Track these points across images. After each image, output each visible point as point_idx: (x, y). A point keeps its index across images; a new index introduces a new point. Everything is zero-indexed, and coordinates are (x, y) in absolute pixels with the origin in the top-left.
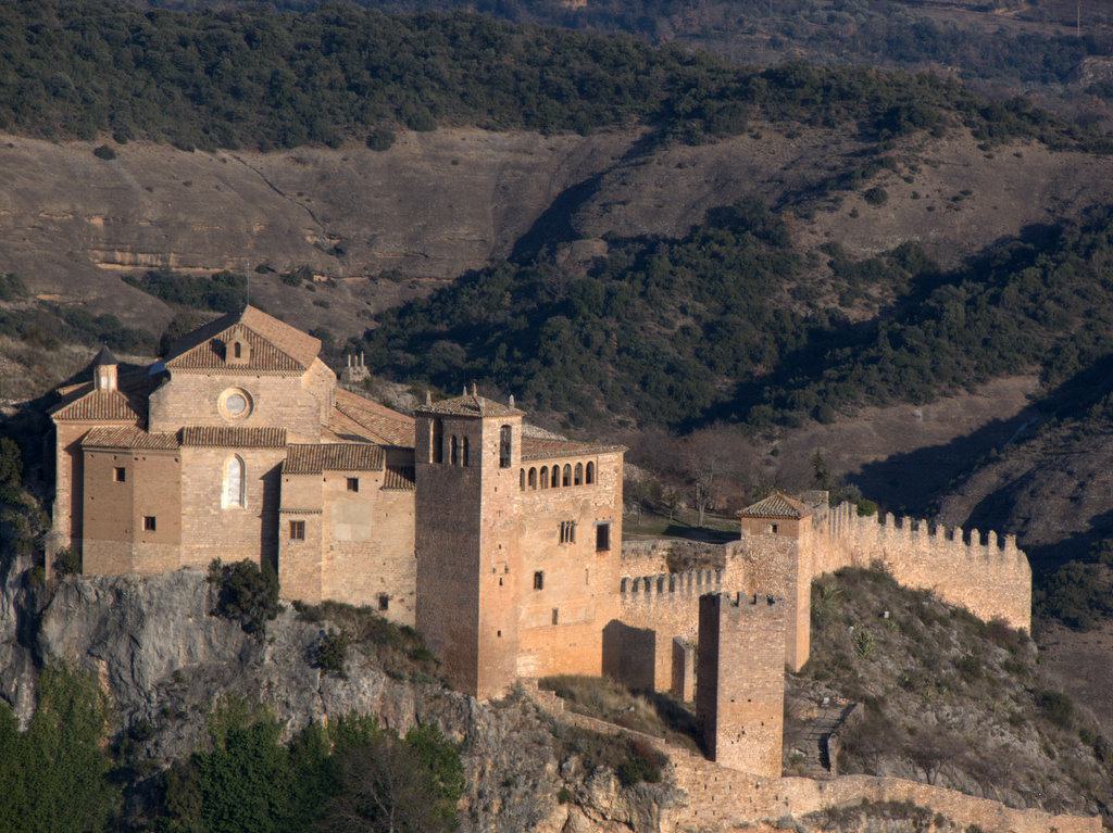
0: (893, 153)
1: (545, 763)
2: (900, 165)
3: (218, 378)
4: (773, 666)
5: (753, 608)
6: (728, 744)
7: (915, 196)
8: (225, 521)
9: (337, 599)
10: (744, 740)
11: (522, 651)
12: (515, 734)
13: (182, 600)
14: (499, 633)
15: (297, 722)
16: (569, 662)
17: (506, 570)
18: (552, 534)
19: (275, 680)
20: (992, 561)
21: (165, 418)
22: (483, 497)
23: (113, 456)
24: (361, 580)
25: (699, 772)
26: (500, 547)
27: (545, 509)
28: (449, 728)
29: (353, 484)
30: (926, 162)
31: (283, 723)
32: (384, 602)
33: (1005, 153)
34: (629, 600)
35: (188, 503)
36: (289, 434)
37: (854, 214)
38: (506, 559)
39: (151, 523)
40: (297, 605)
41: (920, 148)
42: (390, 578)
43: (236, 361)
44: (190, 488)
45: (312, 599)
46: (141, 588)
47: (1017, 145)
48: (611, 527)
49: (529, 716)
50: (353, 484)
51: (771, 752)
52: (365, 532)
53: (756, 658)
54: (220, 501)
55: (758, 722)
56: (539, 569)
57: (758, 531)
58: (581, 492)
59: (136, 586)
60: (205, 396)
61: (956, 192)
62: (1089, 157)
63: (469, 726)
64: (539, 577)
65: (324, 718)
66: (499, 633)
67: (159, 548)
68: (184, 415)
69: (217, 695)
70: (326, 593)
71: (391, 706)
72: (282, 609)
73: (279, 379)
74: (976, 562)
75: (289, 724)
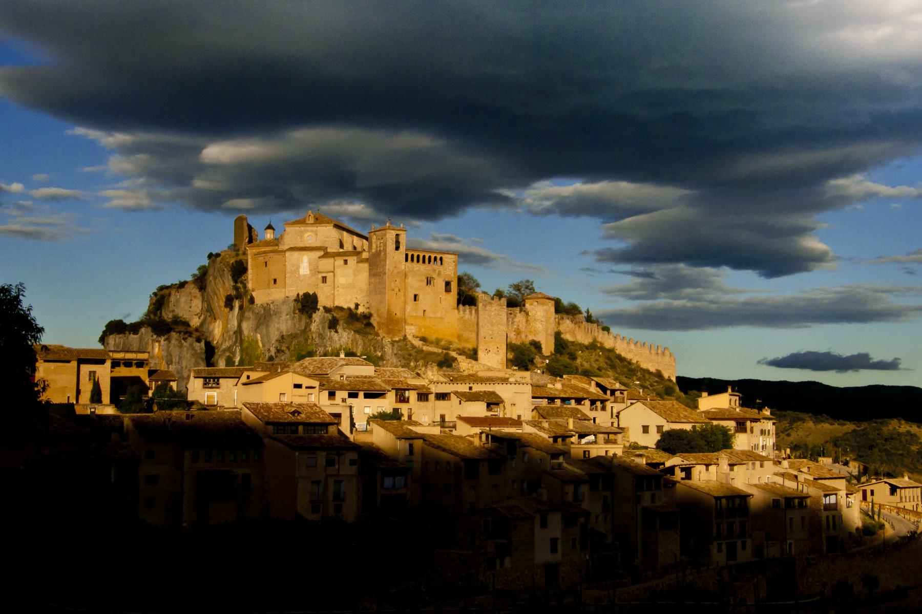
0: (793, 426)
1: (410, 362)
2: (794, 429)
3: (303, 228)
4: (501, 325)
5: (493, 302)
6: (483, 355)
7: (798, 435)
8: (301, 279)
9: (340, 305)
10: (490, 354)
11: (408, 324)
12: (400, 352)
13: (285, 309)
14: (396, 314)
15: (322, 351)
16: (432, 332)
17: (399, 290)
18: (423, 281)
19: (314, 336)
20: (660, 355)
21: (284, 244)
22: (387, 260)
23: (263, 258)
24: (349, 298)
25: (470, 365)
26: (396, 281)
27: (418, 270)
28: (375, 351)
29: (346, 262)
30: (801, 428)
31: (316, 351)
32: (357, 305)
33: (820, 426)
34: (461, 312)
35: (288, 273)
36: (328, 248)
37: (783, 438)
38: (399, 286)
39: (275, 281)
40: (325, 308)
41: (800, 425)
42: (359, 297)
43: (309, 222)
44: (289, 267)
45: (329, 304)
46: (271, 306)
47: (823, 424)
48: (452, 283)
49: (407, 347)
50: (346, 262)
51: (502, 359)
52: (350, 280)
53: (494, 321)
54: (299, 272)
55: (495, 347)
56: (416, 293)
57: (531, 304)
58: (437, 266)
59: (270, 305)
60: (298, 235)
61: (808, 434)
62: (840, 426)
63: (383, 349)
64: (415, 296)
65: (330, 349)
66: (396, 314)
67: (277, 290)
68: (291, 243)
69: (294, 343)
70: (337, 303)
71: (355, 343)
72: (319, 310)
73: (324, 228)
74: (653, 355)
75: (318, 352)
